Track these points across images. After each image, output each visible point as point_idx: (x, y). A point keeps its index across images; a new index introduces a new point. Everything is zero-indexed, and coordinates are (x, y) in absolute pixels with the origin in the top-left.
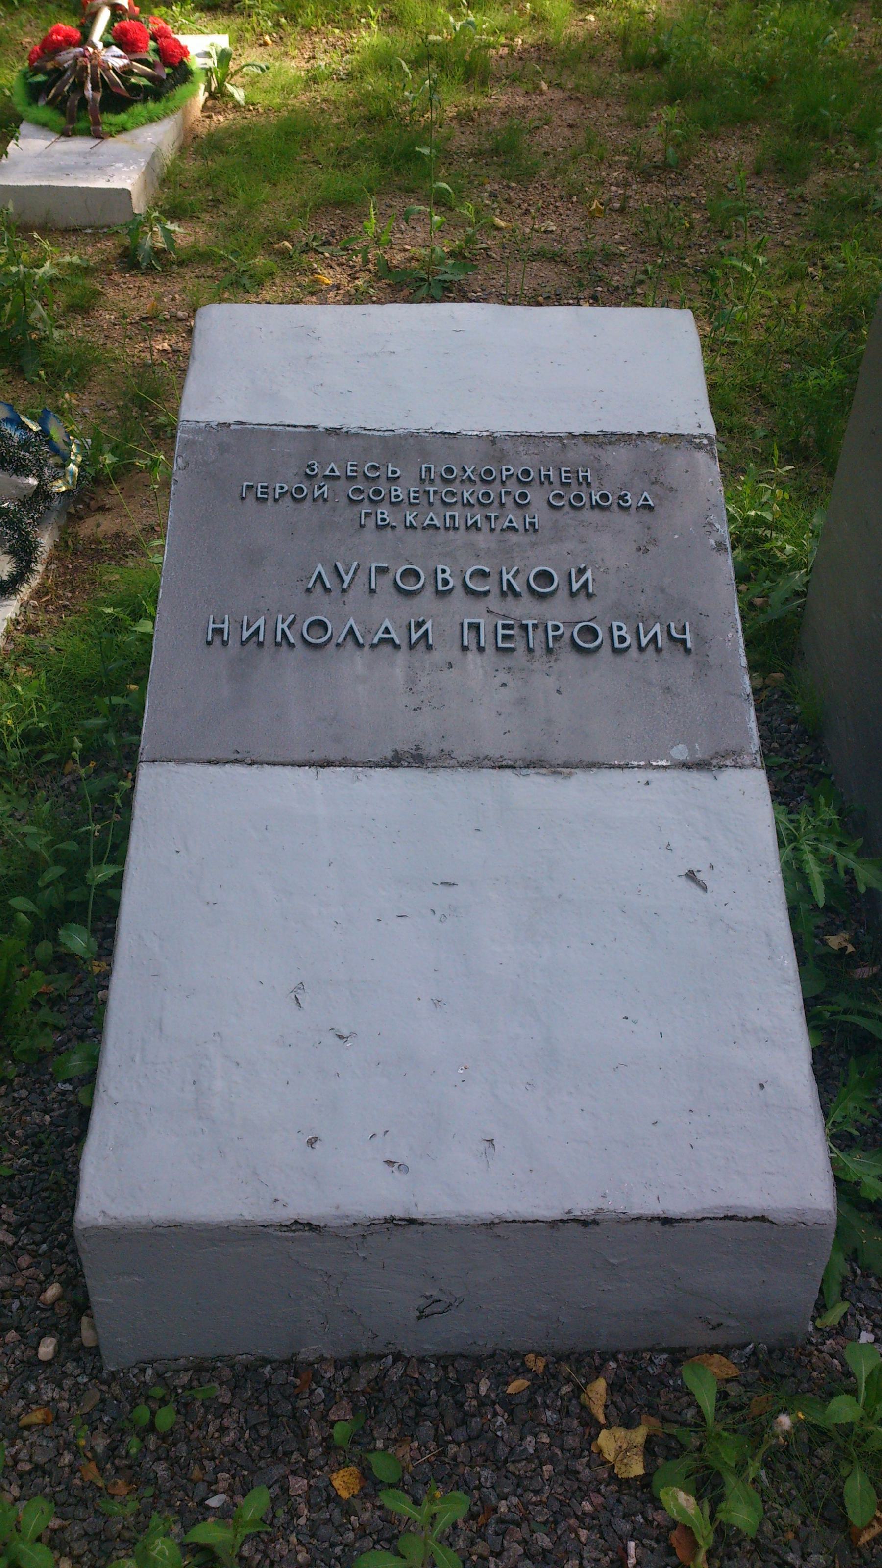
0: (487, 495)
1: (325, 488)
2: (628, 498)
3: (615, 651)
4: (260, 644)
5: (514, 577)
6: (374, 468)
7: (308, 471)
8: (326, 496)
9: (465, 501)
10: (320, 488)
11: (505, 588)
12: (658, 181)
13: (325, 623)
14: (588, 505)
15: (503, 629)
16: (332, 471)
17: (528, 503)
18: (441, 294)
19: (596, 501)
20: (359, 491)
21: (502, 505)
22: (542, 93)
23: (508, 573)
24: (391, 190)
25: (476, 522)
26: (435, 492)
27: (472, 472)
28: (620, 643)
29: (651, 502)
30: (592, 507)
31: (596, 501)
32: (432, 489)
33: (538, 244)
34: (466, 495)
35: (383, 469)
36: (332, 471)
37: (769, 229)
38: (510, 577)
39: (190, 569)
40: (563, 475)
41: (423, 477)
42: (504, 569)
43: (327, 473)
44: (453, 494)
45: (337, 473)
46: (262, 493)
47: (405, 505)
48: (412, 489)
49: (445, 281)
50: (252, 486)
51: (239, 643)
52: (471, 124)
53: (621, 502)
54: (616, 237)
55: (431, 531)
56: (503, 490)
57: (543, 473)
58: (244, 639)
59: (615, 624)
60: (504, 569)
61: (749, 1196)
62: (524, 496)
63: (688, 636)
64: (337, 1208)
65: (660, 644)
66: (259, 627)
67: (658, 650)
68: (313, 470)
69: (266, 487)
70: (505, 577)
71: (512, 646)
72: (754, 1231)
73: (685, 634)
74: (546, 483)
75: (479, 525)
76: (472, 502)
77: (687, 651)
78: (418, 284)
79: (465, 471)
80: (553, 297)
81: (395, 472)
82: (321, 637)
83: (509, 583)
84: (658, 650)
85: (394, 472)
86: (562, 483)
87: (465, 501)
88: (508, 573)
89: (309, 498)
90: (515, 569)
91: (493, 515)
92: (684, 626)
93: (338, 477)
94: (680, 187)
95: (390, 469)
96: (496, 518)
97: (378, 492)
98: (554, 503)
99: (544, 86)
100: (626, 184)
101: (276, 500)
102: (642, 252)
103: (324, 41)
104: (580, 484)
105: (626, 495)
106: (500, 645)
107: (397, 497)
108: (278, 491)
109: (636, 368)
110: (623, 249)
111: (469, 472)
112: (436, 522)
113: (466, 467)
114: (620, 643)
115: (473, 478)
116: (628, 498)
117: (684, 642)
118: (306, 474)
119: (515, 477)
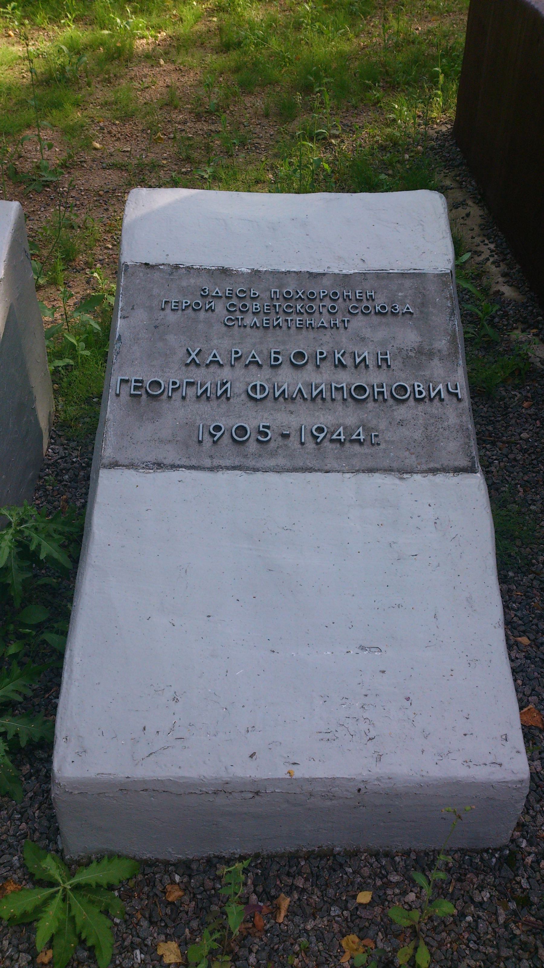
0: (333, 307)
1: (213, 303)
3: (416, 400)
4: (208, 398)
5: (342, 356)
6: (242, 291)
7: (202, 293)
8: (213, 308)
9: (298, 311)
10: (210, 303)
11: (337, 362)
12: (205, 121)
13: (405, 386)
16: (217, 293)
18: (41, 189)
20: (233, 305)
21: (321, 313)
22: (161, 66)
23: (338, 353)
24: (254, 120)
25: (279, 323)
26: (280, 306)
29: (411, 310)
30: (376, 313)
33: (118, 159)
34: (299, 307)
35: (248, 292)
36: (217, 293)
37: (258, 151)
38: (339, 355)
40: (358, 295)
41: (272, 297)
42: (336, 351)
43: (214, 294)
44: (291, 307)
45: (220, 295)
46: (359, 296)
48: (265, 304)
49: (47, 181)
51: (195, 396)
52: (108, 85)
53: (393, 310)
54: (165, 155)
55: (322, 329)
56: (321, 304)
57: (345, 294)
58: (218, 395)
59: (416, 384)
60: (336, 351)
65: (443, 397)
66: (207, 388)
68: (205, 292)
70: (337, 356)
71: (140, 393)
73: (383, 388)
74: (347, 300)
75: (281, 325)
76: (302, 311)
78: (30, 182)
79: (298, 293)
80: (110, 191)
81: (255, 294)
82: (404, 395)
83: (339, 359)
84: (441, 400)
85: (255, 294)
86: (357, 300)
87: (298, 311)
88: (338, 353)
89: (250, 311)
90: (343, 351)
91: (346, 319)
92: (456, 385)
93: (221, 297)
94: (216, 125)
95: (252, 292)
96: (348, 321)
97: (244, 306)
98: (364, 311)
99: (162, 62)
100: (185, 123)
101: (183, 310)
102: (176, 165)
103: (46, 34)
104: (367, 300)
105: (396, 306)
107: (256, 309)
108: (184, 305)
110: (165, 162)
111: (300, 294)
112: (325, 325)
113: (298, 291)
115: (303, 297)
117: (457, 394)
118: (201, 294)
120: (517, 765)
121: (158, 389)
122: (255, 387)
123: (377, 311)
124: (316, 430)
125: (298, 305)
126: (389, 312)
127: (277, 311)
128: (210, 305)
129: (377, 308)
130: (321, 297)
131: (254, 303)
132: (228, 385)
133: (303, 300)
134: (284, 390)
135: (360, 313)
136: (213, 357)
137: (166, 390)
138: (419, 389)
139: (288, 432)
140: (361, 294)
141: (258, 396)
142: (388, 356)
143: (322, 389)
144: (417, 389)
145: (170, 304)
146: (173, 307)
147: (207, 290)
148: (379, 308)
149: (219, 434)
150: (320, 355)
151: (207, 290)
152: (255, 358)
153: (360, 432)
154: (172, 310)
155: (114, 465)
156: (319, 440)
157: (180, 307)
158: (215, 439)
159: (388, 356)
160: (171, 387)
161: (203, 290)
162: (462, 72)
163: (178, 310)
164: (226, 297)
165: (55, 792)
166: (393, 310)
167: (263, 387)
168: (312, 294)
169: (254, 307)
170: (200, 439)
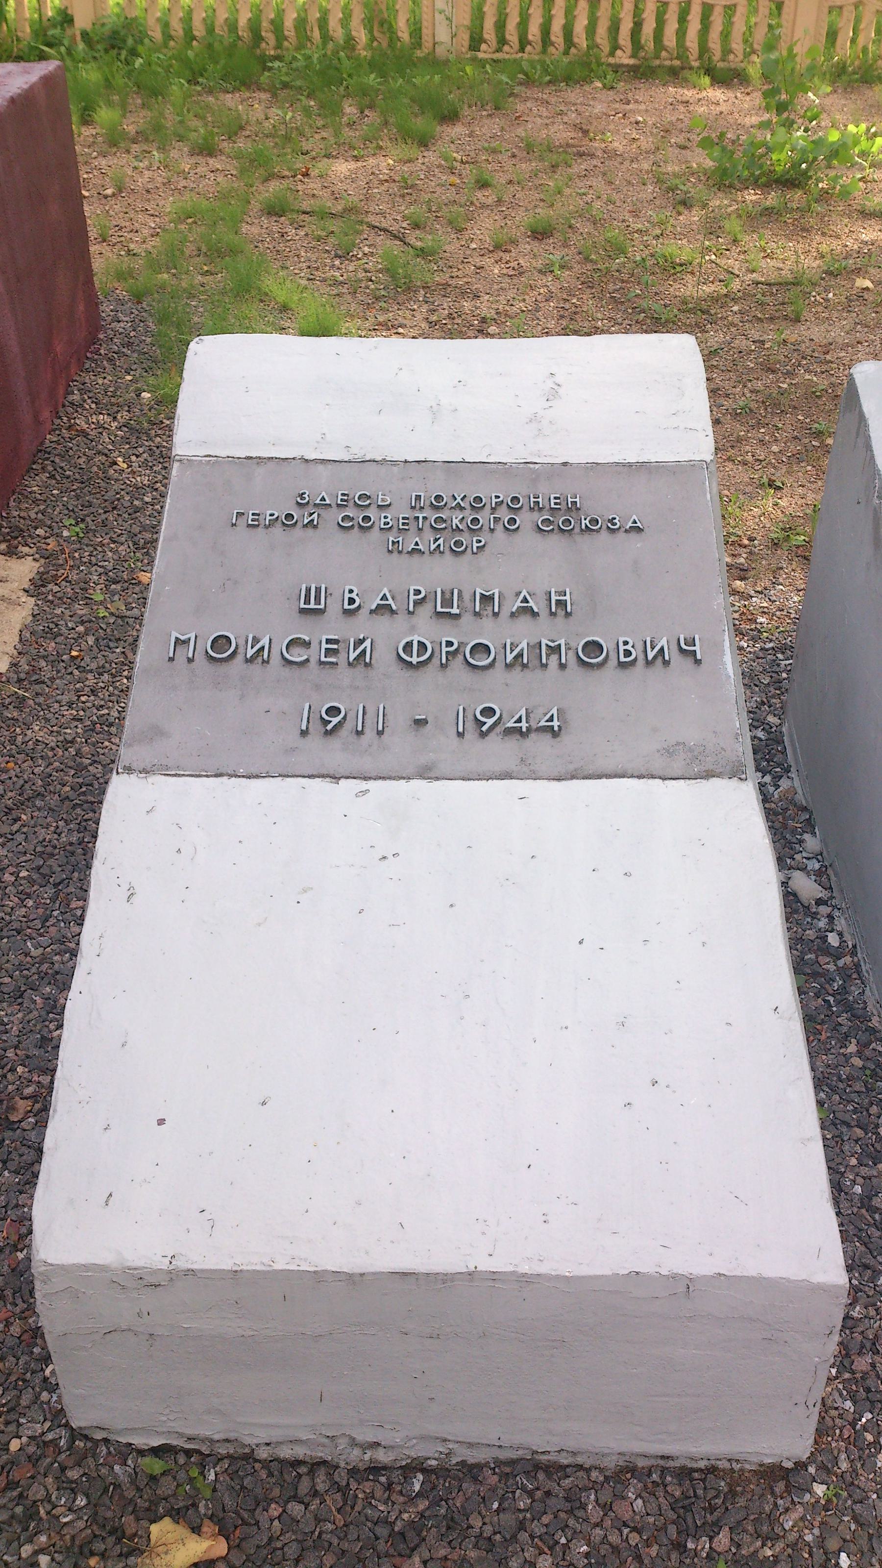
0: (475, 521)
1: (315, 515)
2: (616, 521)
4: (524, 666)
9: (454, 527)
10: (311, 514)
14: (577, 530)
15: (327, 643)
17: (518, 528)
19: (586, 526)
20: (346, 518)
26: (425, 518)
27: (462, 500)
28: (625, 657)
31: (586, 526)
32: (421, 516)
36: (323, 499)
39: (189, 584)
43: (318, 502)
45: (328, 502)
47: (395, 530)
50: (243, 514)
53: (609, 525)
61: (820, 1278)
62: (512, 521)
63: (697, 648)
64: (476, 1267)
67: (666, 663)
69: (559, 498)
72: (739, 1308)
77: (698, 662)
87: (454, 527)
106: (323, 659)
108: (268, 518)
109: (630, 399)
111: (459, 500)
114: (625, 657)
115: (462, 504)
116: (616, 521)
119: (505, 505)
120: (810, 1250)
121: (226, 647)
122: (409, 645)
123: (583, 527)
124: (481, 712)
125: (454, 517)
126: (604, 527)
127: (420, 526)
128: (310, 519)
129: (583, 522)
130: (493, 506)
131: (383, 515)
132: (367, 643)
133: (462, 509)
134: (662, 649)
135: (356, 528)
136: (522, 602)
137: (437, 654)
138: (626, 647)
139: (424, 717)
140: (558, 501)
141: (415, 660)
142: (567, 597)
143: (522, 650)
144: (622, 648)
145: (245, 516)
146: (250, 522)
147: (306, 496)
148: (587, 522)
149: (335, 720)
150: (415, 595)
151: (306, 496)
152: (528, 602)
153: (553, 715)
154: (249, 526)
155: (129, 770)
156: (484, 728)
157: (262, 522)
158: (329, 727)
159: (567, 597)
160: (445, 649)
161: (301, 496)
162: (75, 145)
163: (258, 525)
164: (338, 505)
165: (53, 1316)
166: (609, 525)
167: (422, 646)
168: (478, 499)
169: (383, 520)
170: (461, 730)
